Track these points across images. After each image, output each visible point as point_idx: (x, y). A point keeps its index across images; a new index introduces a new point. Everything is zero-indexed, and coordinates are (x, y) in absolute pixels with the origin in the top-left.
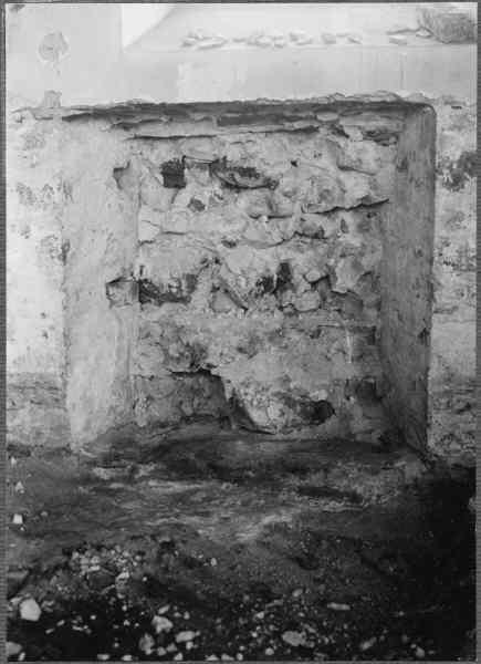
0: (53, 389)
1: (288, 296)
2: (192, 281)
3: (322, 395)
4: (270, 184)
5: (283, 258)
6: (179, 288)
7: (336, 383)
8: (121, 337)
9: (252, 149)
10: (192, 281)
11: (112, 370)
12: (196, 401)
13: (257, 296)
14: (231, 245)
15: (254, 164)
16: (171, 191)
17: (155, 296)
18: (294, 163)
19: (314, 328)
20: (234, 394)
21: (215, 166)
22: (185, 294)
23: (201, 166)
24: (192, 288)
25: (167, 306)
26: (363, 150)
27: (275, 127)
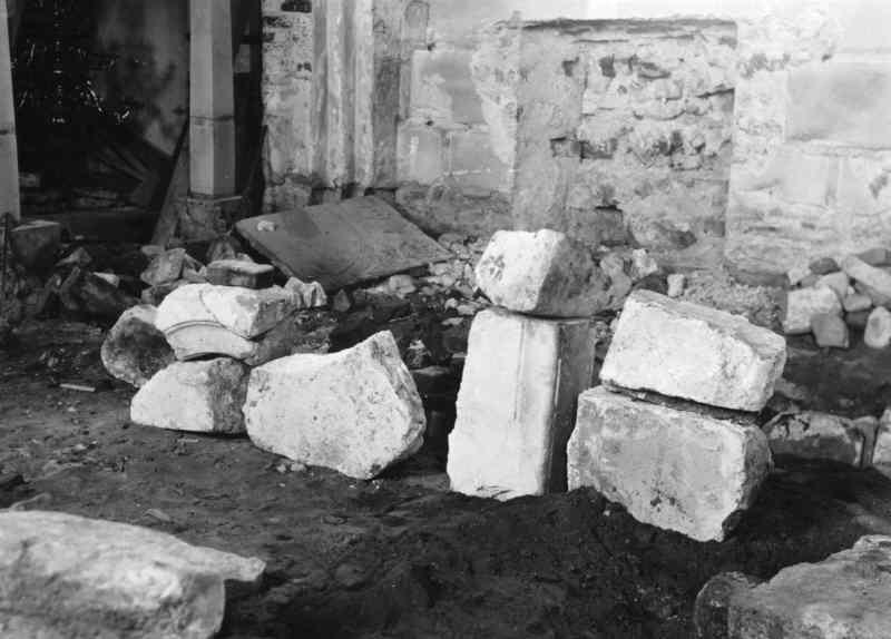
0: (505, 203)
1: (677, 157)
2: (614, 143)
3: (685, 228)
4: (665, 75)
5: (674, 128)
6: (606, 147)
7: (699, 219)
8: (560, 177)
9: (652, 49)
10: (614, 143)
11: (551, 200)
12: (612, 232)
13: (652, 155)
14: (639, 117)
15: (652, 60)
16: (608, 79)
17: (593, 154)
18: (682, 60)
19: (690, 180)
20: (629, 223)
21: (631, 61)
22: (609, 153)
23: (623, 61)
24: (614, 148)
25: (598, 161)
26: (716, 52)
27: (663, 35)
